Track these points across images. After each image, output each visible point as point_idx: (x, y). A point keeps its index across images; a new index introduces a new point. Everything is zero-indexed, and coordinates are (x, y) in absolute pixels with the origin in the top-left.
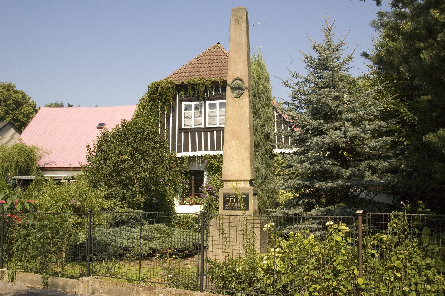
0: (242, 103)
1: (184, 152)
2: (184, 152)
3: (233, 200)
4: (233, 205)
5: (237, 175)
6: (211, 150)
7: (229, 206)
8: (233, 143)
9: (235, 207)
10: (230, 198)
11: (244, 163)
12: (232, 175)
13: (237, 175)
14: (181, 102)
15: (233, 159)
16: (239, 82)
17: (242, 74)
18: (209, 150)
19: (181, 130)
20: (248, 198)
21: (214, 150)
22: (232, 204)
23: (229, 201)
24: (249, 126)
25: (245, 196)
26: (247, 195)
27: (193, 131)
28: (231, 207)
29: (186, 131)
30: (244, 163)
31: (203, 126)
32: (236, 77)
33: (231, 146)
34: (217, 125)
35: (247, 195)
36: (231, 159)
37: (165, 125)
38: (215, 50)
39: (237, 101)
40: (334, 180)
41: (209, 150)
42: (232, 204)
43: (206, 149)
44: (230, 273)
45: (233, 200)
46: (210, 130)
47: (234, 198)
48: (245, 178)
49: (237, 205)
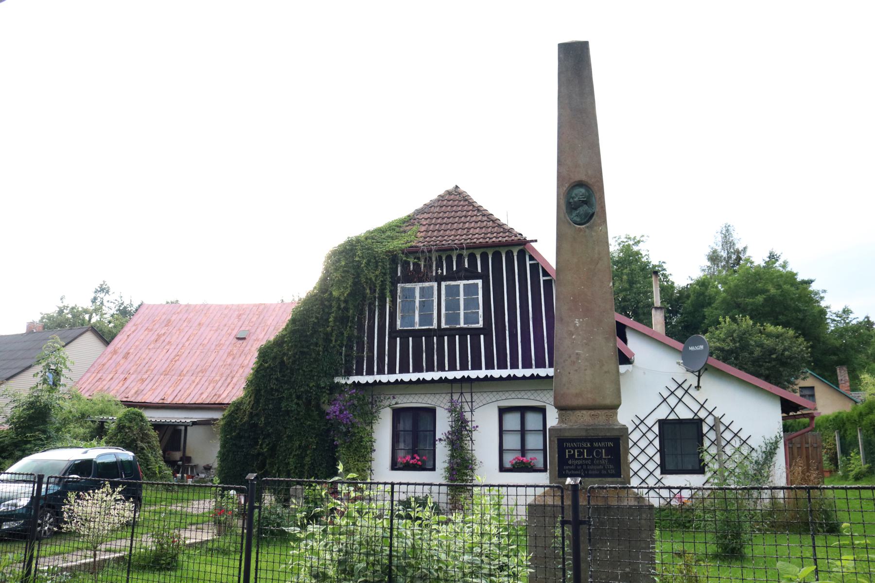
1: (523, 368)
2: (523, 368)
3: (581, 454)
4: (582, 465)
6: (450, 370)
7: (572, 467)
9: (588, 470)
10: (574, 449)
12: (577, 395)
13: (589, 396)
15: (578, 359)
16: (583, 190)
17: (589, 172)
18: (447, 368)
19: (394, 333)
21: (456, 370)
22: (579, 462)
23: (572, 456)
25: (610, 444)
27: (417, 334)
28: (576, 470)
29: (405, 335)
33: (572, 329)
36: (573, 358)
37: (386, 353)
39: (580, 230)
40: (239, 437)
41: (447, 368)
42: (579, 462)
45: (581, 454)
46: (447, 333)
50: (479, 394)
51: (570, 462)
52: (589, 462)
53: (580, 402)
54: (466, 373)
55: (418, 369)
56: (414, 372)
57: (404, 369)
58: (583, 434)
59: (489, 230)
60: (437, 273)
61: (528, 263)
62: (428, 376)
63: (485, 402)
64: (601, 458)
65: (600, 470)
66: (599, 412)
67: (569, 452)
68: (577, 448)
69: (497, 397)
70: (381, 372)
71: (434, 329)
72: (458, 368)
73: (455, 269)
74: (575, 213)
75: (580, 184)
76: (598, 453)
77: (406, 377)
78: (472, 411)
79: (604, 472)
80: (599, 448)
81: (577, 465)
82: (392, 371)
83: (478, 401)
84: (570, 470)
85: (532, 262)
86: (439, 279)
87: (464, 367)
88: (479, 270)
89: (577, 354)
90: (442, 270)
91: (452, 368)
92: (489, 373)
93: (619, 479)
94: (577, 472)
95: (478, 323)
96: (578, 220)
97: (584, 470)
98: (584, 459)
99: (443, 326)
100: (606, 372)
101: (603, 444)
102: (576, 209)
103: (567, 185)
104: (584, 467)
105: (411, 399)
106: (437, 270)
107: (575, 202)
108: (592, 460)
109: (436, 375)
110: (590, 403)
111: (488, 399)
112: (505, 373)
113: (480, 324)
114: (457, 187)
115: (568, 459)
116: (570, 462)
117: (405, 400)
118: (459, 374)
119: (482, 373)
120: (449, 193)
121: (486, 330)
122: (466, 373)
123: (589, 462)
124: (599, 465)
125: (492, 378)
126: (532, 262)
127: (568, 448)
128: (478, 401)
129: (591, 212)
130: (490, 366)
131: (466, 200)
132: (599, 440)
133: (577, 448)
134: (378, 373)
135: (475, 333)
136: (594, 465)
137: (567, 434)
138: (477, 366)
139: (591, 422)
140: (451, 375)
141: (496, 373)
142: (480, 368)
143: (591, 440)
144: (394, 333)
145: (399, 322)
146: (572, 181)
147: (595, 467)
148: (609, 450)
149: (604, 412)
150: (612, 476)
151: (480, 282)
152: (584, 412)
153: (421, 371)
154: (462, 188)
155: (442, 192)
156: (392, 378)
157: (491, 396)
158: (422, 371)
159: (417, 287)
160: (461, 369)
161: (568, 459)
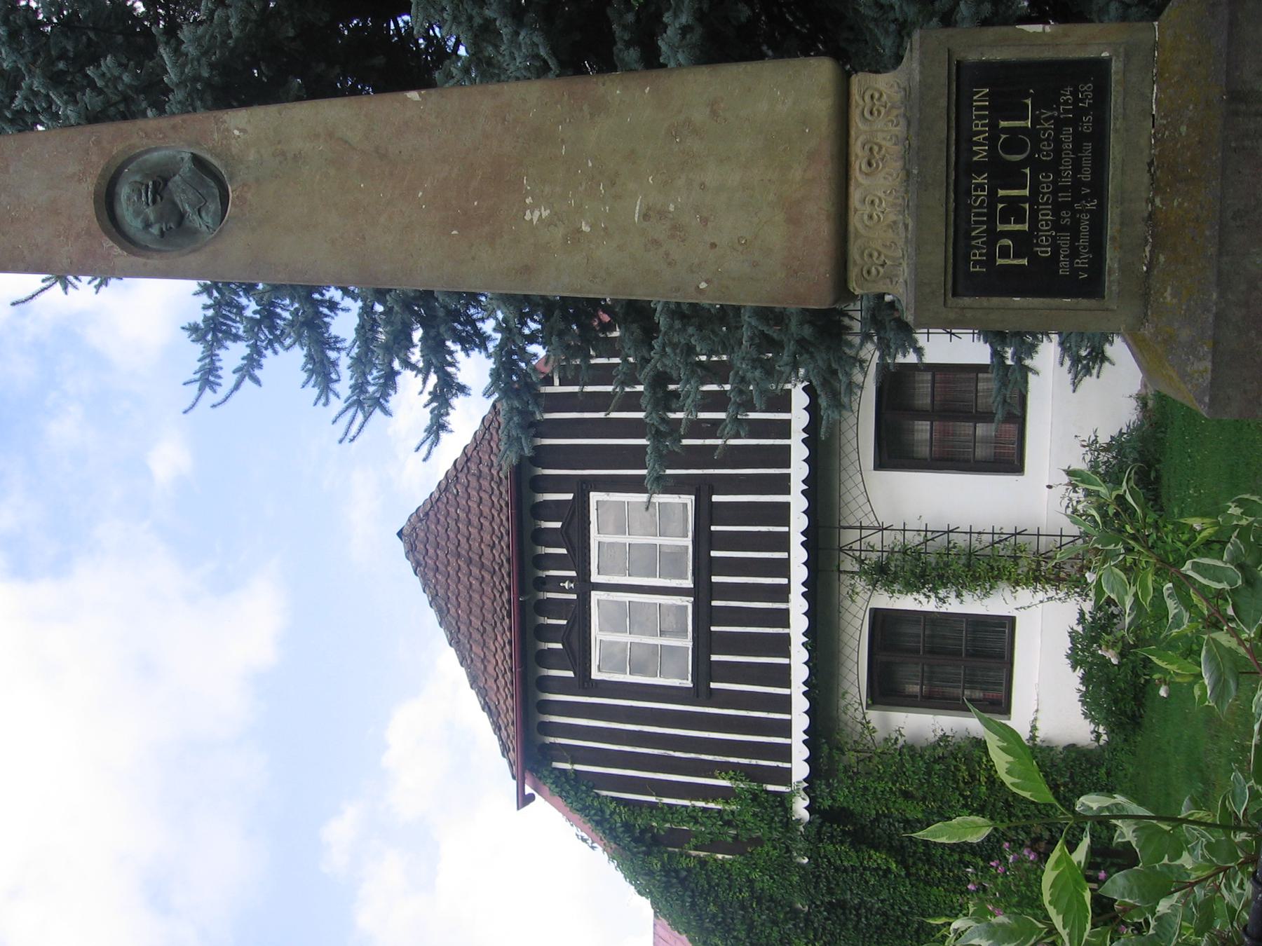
0: (252, 156)
3: (1013, 210)
4: (1057, 208)
5: (797, 174)
7: (1065, 240)
8: (533, 216)
9: (1077, 184)
11: (699, 115)
12: (794, 220)
13: (797, 174)
14: (584, 683)
15: (663, 214)
16: (124, 191)
17: (72, 168)
19: (700, 693)
20: (993, 74)
22: (1046, 216)
23: (1023, 243)
24: (413, 95)
25: (980, 97)
26: (965, 77)
27: (704, 643)
29: (704, 670)
30: (699, 115)
31: (687, 602)
32: (90, 210)
33: (559, 232)
34: (688, 542)
35: (965, 77)
38: (420, 546)
42: (1046, 216)
43: (782, 593)
44: (907, 795)
45: (1013, 210)
47: (994, 130)
48: (822, 106)
49: (1054, 166)
50: (845, 511)
51: (1045, 252)
52: (1046, 179)
53: (819, 206)
54: (797, 539)
55: (782, 645)
56: (788, 655)
57: (782, 676)
58: (937, 197)
59: (485, 470)
60: (570, 591)
61: (557, 388)
62: (799, 624)
63: (862, 500)
64: (1033, 133)
65: (1078, 138)
66: (857, 148)
67: (1005, 253)
68: (991, 216)
69: (852, 470)
70: (785, 729)
71: (695, 605)
72: (784, 555)
73: (564, 551)
74: (195, 221)
75: (107, 200)
76: (1015, 141)
77: (800, 673)
78: (882, 529)
79: (1087, 124)
80: (992, 140)
81: (1057, 226)
82: (785, 704)
83: (860, 514)
84: (1074, 253)
85: (557, 381)
86: (585, 586)
87: (782, 542)
88: (569, 496)
89: (645, 216)
90: (564, 579)
91: (782, 568)
92: (797, 485)
93: (1115, 66)
94: (1084, 228)
95: (685, 505)
96: (214, 206)
97: (1077, 197)
98: (1033, 199)
99: (688, 583)
100: (714, 113)
101: (979, 126)
102: (182, 216)
103: (107, 243)
104: (1064, 197)
105: (850, 664)
106: (563, 590)
107: (160, 218)
108: (1037, 166)
109: (797, 606)
110: (825, 171)
111: (855, 492)
112: (799, 452)
113: (689, 500)
114: (400, 534)
115: (1033, 258)
116: (1045, 252)
117: (854, 690)
118: (798, 555)
119: (797, 502)
120: (411, 551)
121: (702, 489)
122: (797, 539)
123: (1046, 179)
124: (1058, 142)
125: (812, 429)
126: (557, 381)
127: (991, 257)
128: (860, 514)
129: (187, 166)
130: (782, 484)
131: (427, 514)
132: (962, 137)
133: (991, 216)
134: (788, 734)
135: (706, 514)
136: (1058, 159)
137: (937, 257)
138: (781, 514)
139: (896, 166)
140: (799, 573)
141: (798, 470)
142: (787, 505)
143: (963, 169)
144: (700, 693)
145: (675, 682)
146: (96, 225)
147: (1067, 159)
148: (1003, 105)
149: (858, 125)
150: (1102, 93)
151: (595, 497)
152: (855, 196)
153: (786, 639)
154: (402, 522)
155: (408, 566)
156: (800, 704)
157: (849, 484)
158: (787, 638)
159: (598, 634)
160: (787, 548)
161: (1033, 258)
